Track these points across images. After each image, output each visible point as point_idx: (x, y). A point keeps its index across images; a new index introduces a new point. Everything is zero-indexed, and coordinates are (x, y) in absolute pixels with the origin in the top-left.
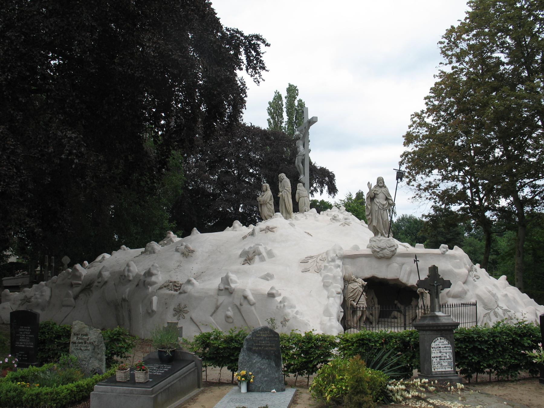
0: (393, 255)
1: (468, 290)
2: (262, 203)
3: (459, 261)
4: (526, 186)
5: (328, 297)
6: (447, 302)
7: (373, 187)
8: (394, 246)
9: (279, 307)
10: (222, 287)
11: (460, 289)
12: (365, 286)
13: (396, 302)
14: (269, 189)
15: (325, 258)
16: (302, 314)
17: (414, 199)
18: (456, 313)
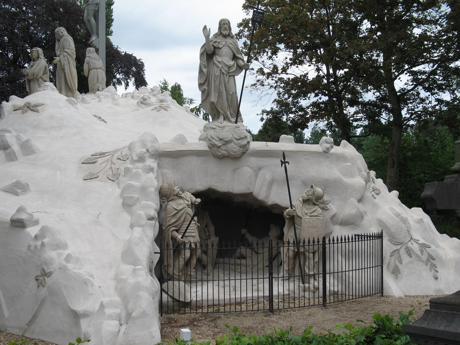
1: (366, 213)
2: (30, 77)
4: (406, 72)
5: (132, 226)
6: (331, 233)
7: (211, 36)
9: (32, 248)
11: (354, 211)
12: (197, 205)
13: (243, 231)
15: (126, 155)
16: (77, 260)
17: (254, 87)
18: (347, 250)
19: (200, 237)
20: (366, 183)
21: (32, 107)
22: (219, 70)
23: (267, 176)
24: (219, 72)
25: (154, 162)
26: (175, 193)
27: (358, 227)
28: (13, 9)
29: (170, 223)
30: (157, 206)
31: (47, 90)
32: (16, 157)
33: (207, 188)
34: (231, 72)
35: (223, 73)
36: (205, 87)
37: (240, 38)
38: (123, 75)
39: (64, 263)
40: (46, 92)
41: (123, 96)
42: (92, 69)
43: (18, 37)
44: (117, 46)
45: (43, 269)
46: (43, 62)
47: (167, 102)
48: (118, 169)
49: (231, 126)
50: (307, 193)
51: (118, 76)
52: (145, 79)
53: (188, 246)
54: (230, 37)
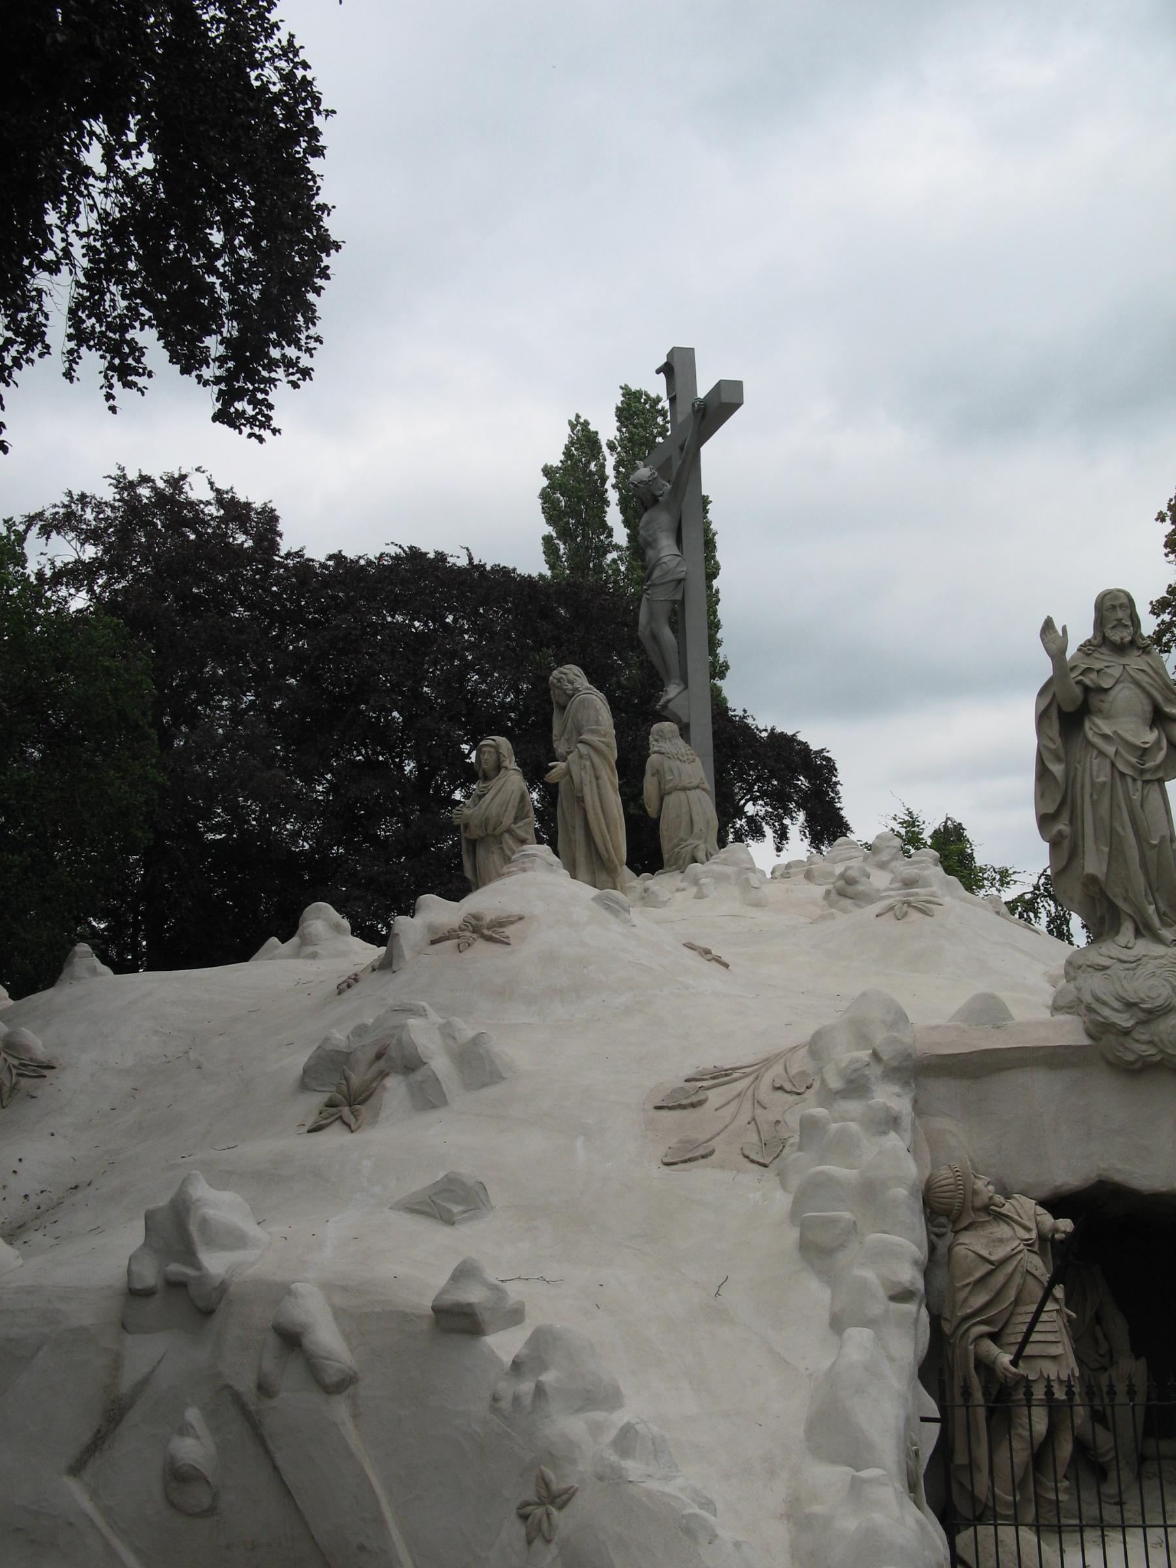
2: (475, 833)
5: (837, 1324)
7: (1071, 651)
9: (505, 1405)
10: (149, 1276)
12: (1062, 1242)
14: (514, 765)
15: (802, 1074)
16: (658, 1448)
19: (1080, 1361)
21: (488, 929)
22: (1108, 763)
24: (1108, 769)
25: (899, 1096)
26: (979, 1202)
28: (417, 624)
30: (919, 1247)
31: (532, 869)
32: (444, 1094)
33: (1091, 1182)
34: (1149, 770)
35: (1122, 775)
36: (1062, 826)
37: (1165, 652)
38: (766, 804)
39: (614, 1458)
40: (529, 875)
41: (777, 874)
42: (670, 793)
43: (432, 708)
44: (745, 711)
45: (543, 1479)
46: (513, 780)
47: (927, 884)
48: (778, 1122)
49: (1162, 957)
51: (750, 809)
52: (842, 813)
53: (1039, 1393)
54: (1139, 648)
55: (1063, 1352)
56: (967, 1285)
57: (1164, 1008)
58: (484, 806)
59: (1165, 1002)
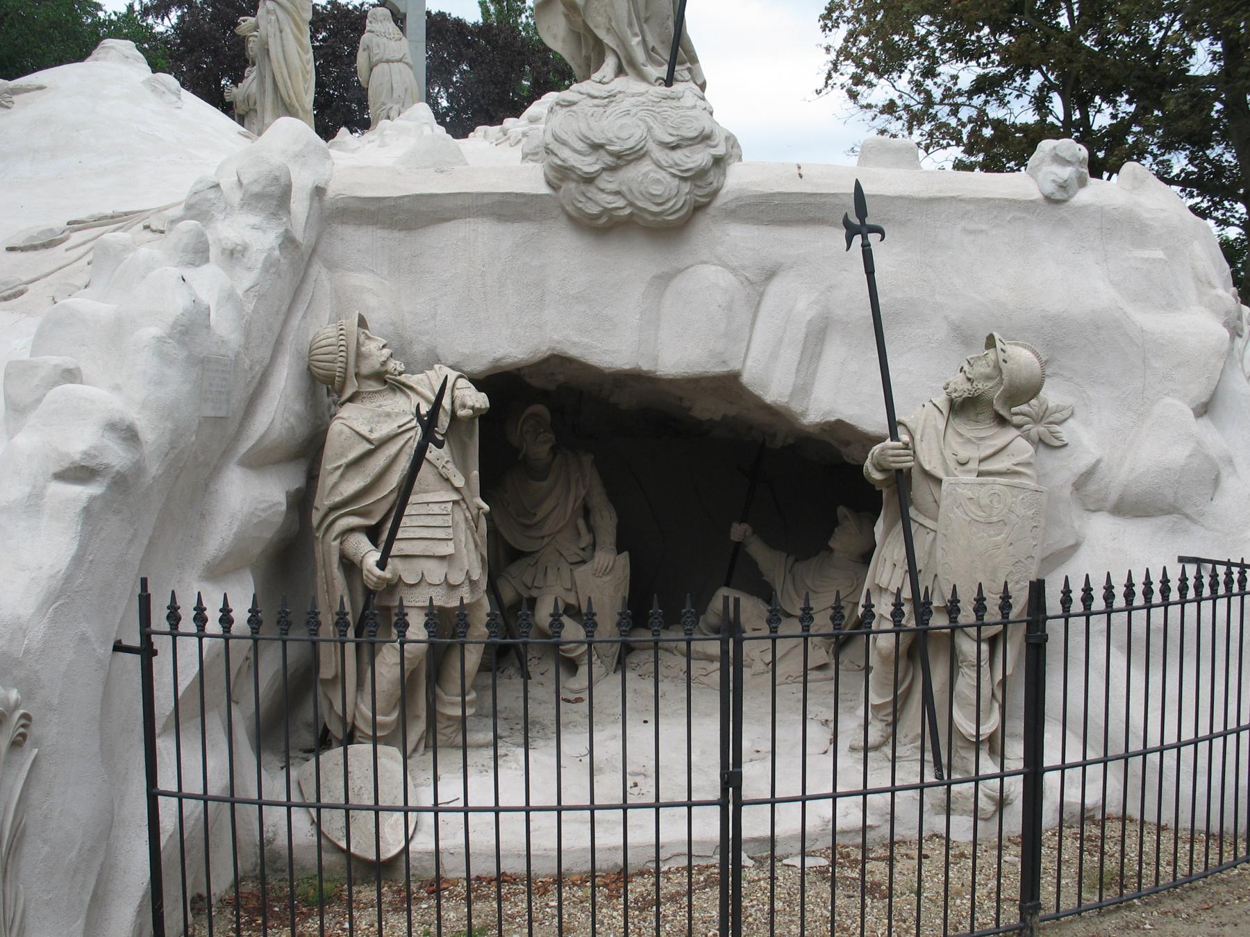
0: (699, 208)
1: (1230, 462)
3: (1160, 254)
8: (705, 138)
11: (1178, 455)
13: (738, 531)
20: (1232, 339)
23: (801, 305)
26: (366, 369)
27: (1194, 521)
29: (338, 499)
42: (376, 65)
49: (642, 94)
50: (966, 368)
55: (453, 552)
56: (338, 467)
57: (636, 152)
58: (247, 85)
59: (637, 145)
